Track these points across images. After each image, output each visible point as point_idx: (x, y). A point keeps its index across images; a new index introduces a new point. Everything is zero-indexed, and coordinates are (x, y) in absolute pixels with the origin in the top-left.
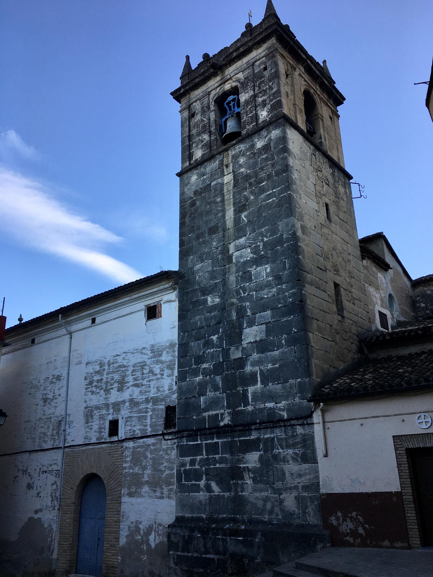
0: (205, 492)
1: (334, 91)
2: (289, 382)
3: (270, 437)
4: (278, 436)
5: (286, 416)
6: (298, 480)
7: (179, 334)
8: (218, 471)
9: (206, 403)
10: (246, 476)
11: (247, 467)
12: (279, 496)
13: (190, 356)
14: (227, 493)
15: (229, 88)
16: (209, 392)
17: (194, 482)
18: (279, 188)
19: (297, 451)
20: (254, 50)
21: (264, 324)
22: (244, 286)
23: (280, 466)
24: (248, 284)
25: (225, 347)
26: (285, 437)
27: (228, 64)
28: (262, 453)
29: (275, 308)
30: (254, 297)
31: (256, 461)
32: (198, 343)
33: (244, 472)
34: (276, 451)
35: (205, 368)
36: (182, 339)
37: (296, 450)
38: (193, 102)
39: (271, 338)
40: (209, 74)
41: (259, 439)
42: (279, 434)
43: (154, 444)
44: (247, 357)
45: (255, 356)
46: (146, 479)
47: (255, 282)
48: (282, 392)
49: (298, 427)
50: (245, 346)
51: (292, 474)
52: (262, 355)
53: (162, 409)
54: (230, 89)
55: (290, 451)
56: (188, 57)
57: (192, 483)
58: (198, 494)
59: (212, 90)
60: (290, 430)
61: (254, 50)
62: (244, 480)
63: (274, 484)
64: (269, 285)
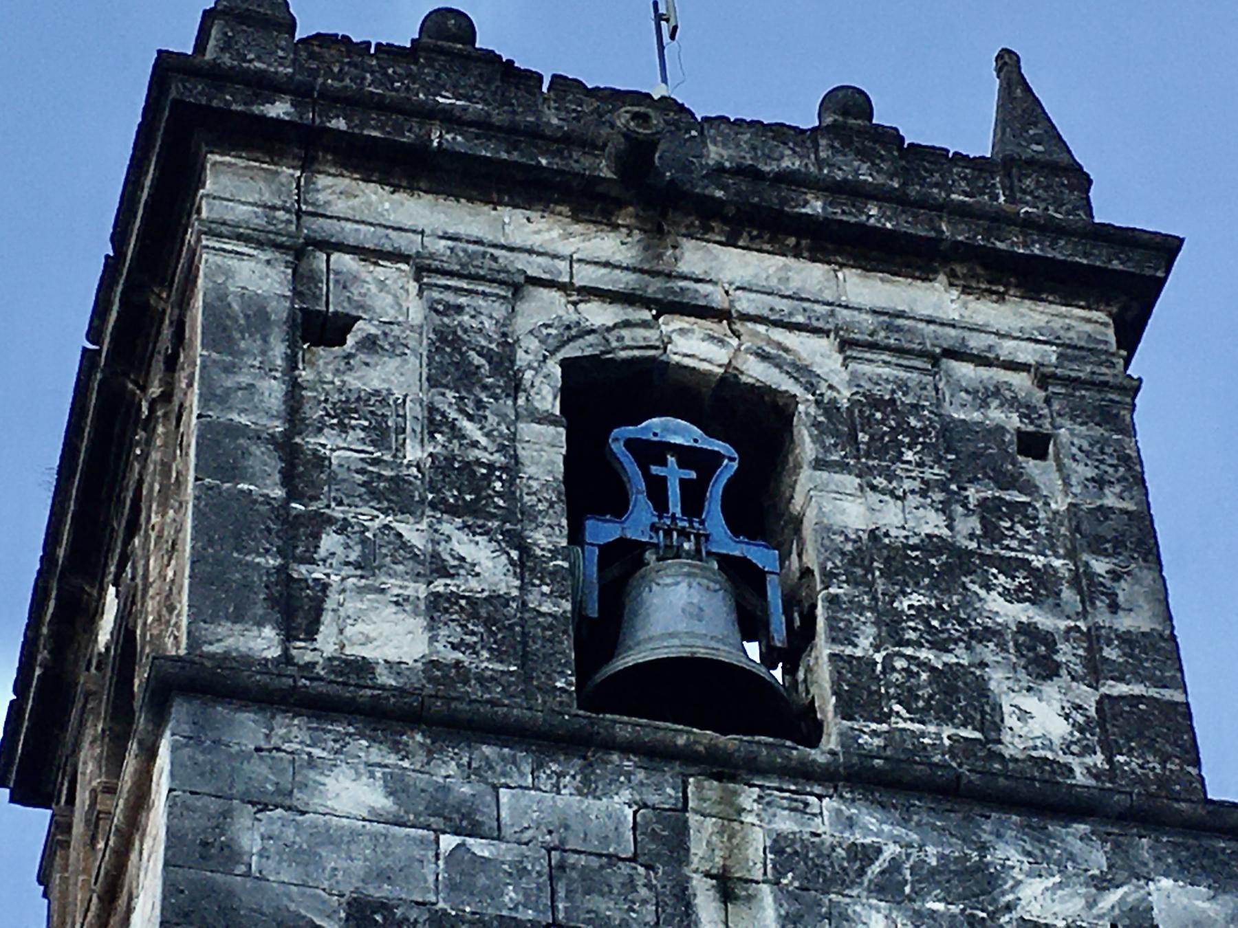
1: (61, 552)
15: (705, 366)
20: (942, 277)
27: (725, 220)
38: (351, 241)
40: (559, 172)
54: (707, 375)
56: (1008, 62)
61: (942, 277)
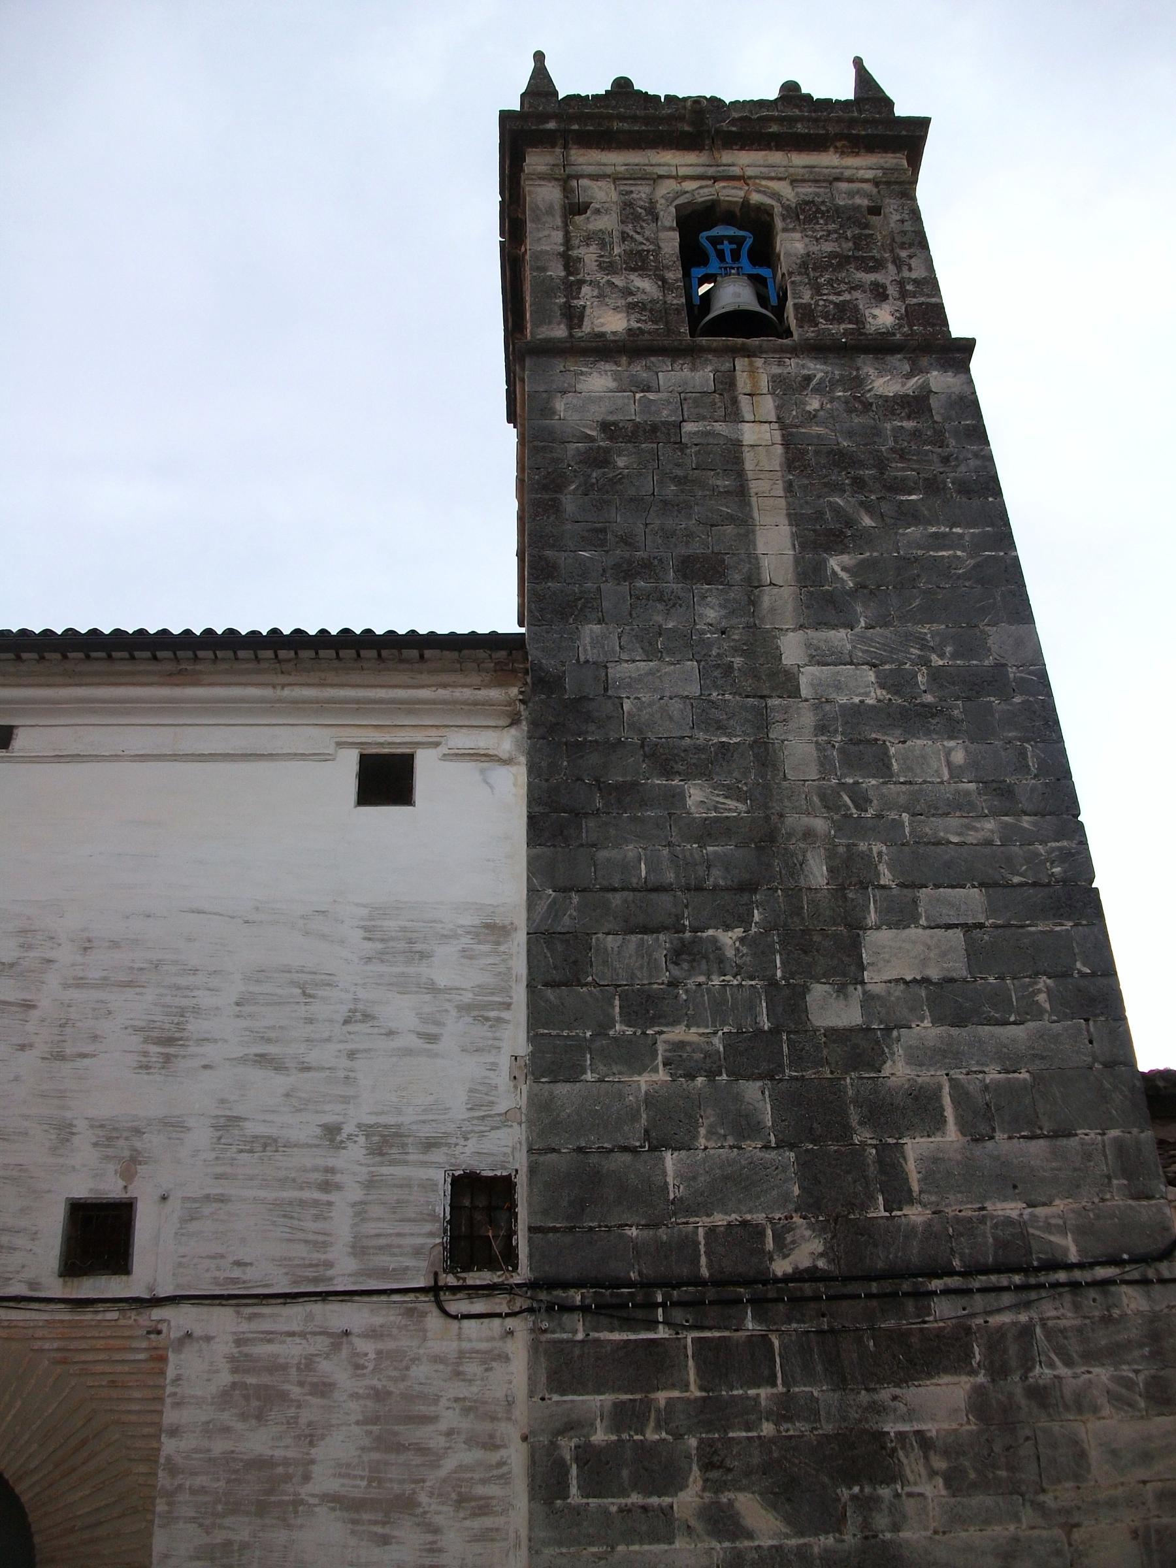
0: (706, 1538)
2: (1076, 1135)
3: (1014, 1324)
4: (1048, 1319)
5: (1073, 1249)
6: (1141, 1473)
7: (531, 890)
8: (771, 1452)
9: (694, 1178)
10: (911, 1463)
11: (918, 1433)
12: (1069, 1534)
13: (597, 985)
14: (822, 1538)
16: (708, 1140)
17: (635, 1498)
18: (977, 531)
19: (1126, 1371)
20: (832, 149)
21: (956, 926)
22: (856, 783)
23: (1061, 1427)
24: (874, 782)
25: (783, 978)
26: (1078, 1322)
28: (981, 1379)
29: (996, 885)
30: (907, 830)
31: (956, 1410)
32: (641, 943)
33: (901, 1453)
34: (1041, 1373)
35: (680, 1045)
36: (555, 910)
37: (1125, 1367)
39: (991, 980)
41: (963, 1332)
42: (1053, 1313)
43: (373, 1334)
44: (888, 1030)
45: (926, 1031)
46: (324, 1481)
47: (902, 783)
48: (1052, 1169)
49: (1124, 1288)
50: (877, 989)
51: (1114, 1453)
52: (954, 1031)
53: (429, 1186)
55: (1102, 1374)
57: (629, 1501)
58: (666, 1547)
59: (669, 177)
60: (1094, 1300)
61: (832, 149)
62: (905, 1482)
63: (1044, 1491)
64: (960, 805)
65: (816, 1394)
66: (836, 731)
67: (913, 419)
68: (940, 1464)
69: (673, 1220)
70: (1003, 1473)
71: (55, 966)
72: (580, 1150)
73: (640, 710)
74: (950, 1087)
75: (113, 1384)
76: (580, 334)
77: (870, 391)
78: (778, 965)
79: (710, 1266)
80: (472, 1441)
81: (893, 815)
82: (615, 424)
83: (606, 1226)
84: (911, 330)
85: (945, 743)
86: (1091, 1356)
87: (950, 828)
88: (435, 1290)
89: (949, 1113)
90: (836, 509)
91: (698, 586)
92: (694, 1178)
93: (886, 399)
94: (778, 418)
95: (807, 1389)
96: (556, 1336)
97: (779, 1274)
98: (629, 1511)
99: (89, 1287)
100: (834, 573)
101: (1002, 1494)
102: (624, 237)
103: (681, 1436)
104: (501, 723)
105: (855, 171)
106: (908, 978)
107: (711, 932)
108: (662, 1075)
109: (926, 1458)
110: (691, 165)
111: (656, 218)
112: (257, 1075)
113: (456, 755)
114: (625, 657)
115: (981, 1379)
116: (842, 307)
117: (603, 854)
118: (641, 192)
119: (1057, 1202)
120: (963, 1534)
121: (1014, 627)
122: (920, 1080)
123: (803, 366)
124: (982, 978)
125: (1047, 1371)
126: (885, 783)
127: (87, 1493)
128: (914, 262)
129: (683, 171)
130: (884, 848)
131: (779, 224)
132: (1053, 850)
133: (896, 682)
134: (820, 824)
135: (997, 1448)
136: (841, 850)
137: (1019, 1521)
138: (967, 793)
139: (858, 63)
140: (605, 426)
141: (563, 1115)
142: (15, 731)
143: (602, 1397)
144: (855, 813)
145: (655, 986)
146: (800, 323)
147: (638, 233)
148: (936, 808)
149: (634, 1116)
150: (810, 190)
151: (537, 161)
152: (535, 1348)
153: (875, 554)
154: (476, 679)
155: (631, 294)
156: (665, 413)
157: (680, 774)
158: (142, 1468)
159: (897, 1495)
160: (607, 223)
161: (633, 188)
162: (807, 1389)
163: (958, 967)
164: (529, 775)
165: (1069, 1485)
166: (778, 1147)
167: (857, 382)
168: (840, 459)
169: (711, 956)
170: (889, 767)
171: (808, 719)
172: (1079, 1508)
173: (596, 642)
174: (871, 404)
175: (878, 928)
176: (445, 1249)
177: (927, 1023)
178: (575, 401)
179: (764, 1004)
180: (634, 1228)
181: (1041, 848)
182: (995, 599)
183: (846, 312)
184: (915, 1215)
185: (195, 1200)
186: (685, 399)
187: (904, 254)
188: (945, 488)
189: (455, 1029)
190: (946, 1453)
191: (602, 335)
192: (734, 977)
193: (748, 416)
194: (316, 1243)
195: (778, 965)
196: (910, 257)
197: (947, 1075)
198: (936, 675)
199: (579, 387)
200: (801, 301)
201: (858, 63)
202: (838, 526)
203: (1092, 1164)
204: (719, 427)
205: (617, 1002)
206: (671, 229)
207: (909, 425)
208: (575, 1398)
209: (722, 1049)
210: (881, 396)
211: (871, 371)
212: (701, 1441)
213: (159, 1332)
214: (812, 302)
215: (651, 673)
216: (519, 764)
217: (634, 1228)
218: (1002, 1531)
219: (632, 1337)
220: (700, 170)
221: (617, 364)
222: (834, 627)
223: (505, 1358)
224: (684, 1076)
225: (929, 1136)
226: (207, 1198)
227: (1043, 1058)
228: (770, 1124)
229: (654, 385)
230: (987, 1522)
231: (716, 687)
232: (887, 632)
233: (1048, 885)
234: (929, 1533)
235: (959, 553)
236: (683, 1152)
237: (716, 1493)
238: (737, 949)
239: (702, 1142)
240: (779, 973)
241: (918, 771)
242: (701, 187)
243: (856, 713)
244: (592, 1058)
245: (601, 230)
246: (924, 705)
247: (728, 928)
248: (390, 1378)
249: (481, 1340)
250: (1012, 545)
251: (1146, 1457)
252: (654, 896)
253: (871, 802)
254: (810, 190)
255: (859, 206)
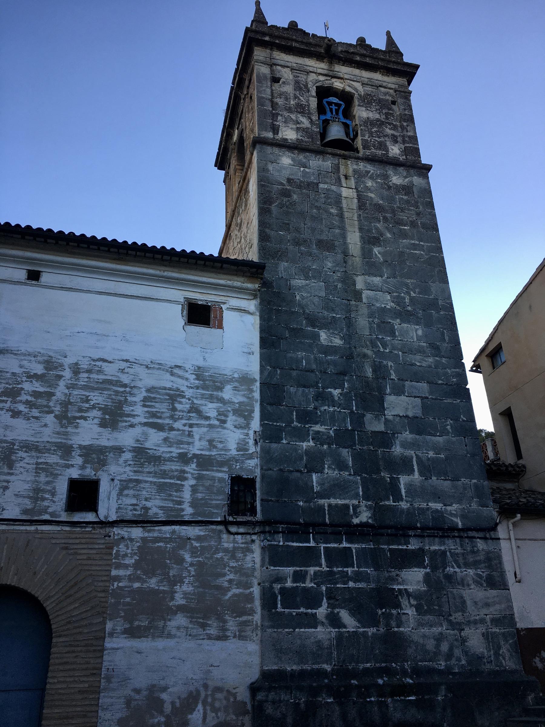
2: (461, 480)
3: (439, 550)
5: (460, 523)
7: (261, 366)
9: (323, 484)
10: (404, 602)
11: (406, 589)
14: (372, 629)
17: (302, 610)
19: (479, 572)
20: (379, 72)
21: (418, 397)
22: (383, 338)
24: (389, 338)
25: (356, 410)
26: (462, 551)
28: (428, 570)
29: (433, 383)
30: (401, 358)
31: (419, 582)
32: (303, 391)
33: (400, 597)
34: (449, 570)
35: (318, 432)
42: (453, 547)
44: (394, 434)
45: (407, 436)
46: (179, 600)
48: (452, 492)
49: (478, 540)
50: (391, 418)
51: (476, 603)
52: (417, 437)
53: (221, 480)
55: (471, 572)
57: (300, 611)
58: (314, 630)
60: (468, 543)
61: (379, 72)
62: (402, 609)
64: (420, 351)
65: (369, 572)
66: (376, 317)
67: (407, 195)
68: (413, 602)
69: (316, 500)
70: (437, 607)
71: (64, 378)
72: (281, 470)
73: (303, 299)
74: (416, 458)
75: (89, 559)
76: (277, 138)
77: (391, 181)
78: (354, 405)
79: (329, 519)
80: (239, 585)
81: (396, 352)
82: (292, 179)
83: (291, 501)
84: (406, 157)
85: (415, 326)
86: (467, 565)
87: (417, 359)
88: (225, 523)
89: (416, 467)
90: (377, 229)
91: (325, 252)
92: (323, 484)
93: (397, 185)
94: (356, 187)
95: (365, 569)
96: (272, 543)
97: (355, 523)
98: (300, 615)
99: (78, 517)
100: (376, 255)
101: (436, 615)
102: (296, 97)
103: (319, 586)
104: (250, 298)
105: (387, 84)
106: (401, 415)
107: (329, 390)
108: (311, 443)
109: (409, 599)
110: (322, 69)
111: (308, 91)
112: (152, 431)
113: (232, 309)
114: (296, 277)
115: (428, 570)
116: (380, 143)
117: (289, 355)
118: (302, 78)
119: (454, 505)
120: (423, 630)
121: (441, 285)
122: (405, 454)
123: (365, 167)
124: (427, 418)
125: (451, 569)
126: (393, 339)
127: (77, 606)
128: (409, 128)
129: (319, 71)
130: (392, 364)
131: (356, 102)
132: (453, 372)
133: (398, 301)
134: (369, 352)
135: (434, 597)
136: (377, 363)
137: (443, 627)
138: (423, 347)
139: (388, 34)
140: (289, 180)
141: (274, 456)
142: (41, 274)
143: (290, 568)
144: (382, 350)
145: (309, 409)
146: (364, 148)
147: (301, 96)
148: (412, 351)
149: (301, 459)
150: (370, 89)
151: (259, 53)
152: (263, 548)
153: (391, 249)
154: (242, 279)
155: (298, 123)
156: (312, 178)
157: (318, 327)
158: (102, 595)
159: (399, 614)
160: (289, 89)
161: (299, 75)
162: (365, 569)
163: (419, 412)
164: (260, 320)
165: (460, 614)
166: (354, 475)
167: (386, 177)
168: (379, 208)
169: (329, 399)
170: (395, 333)
171: (364, 310)
172: (464, 623)
173: (285, 270)
174: (391, 187)
175: (390, 395)
176: (228, 506)
177: (407, 433)
178: (277, 167)
179: (349, 420)
180: (301, 502)
181: (449, 371)
182: (435, 272)
183: (382, 146)
184: (404, 505)
185: (125, 481)
186: (320, 174)
187: (405, 124)
188: (418, 226)
189: (231, 419)
190: (415, 598)
191: (286, 139)
192: (338, 408)
193: (345, 185)
194: (176, 501)
195: (354, 405)
196: (408, 126)
197: (415, 453)
198: (412, 299)
199: (278, 161)
200: (364, 138)
201: (388, 34)
202: (378, 236)
203: (466, 492)
204: (334, 188)
205: (295, 413)
206: (313, 97)
207: (405, 197)
208: (280, 568)
209: (333, 435)
210: (395, 184)
211: (392, 173)
212: (327, 588)
213: (110, 536)
214: (369, 139)
215: (307, 285)
216: (256, 315)
217: (301, 502)
218: (436, 630)
219: (301, 545)
220: (325, 72)
221: (293, 153)
222: (376, 276)
223: (252, 552)
224: (320, 444)
225: (408, 476)
226: (131, 480)
227: (449, 450)
228: (351, 466)
229: (308, 165)
230: (431, 626)
231: (332, 294)
232: (395, 280)
233: (451, 385)
234: (410, 629)
235: (422, 253)
236: (319, 474)
237: (333, 609)
238: (339, 397)
239: (326, 471)
240: (354, 408)
241: (405, 336)
242: (327, 80)
243: (383, 310)
244: (285, 435)
245: (285, 91)
246: (408, 311)
247: (335, 389)
248: (206, 558)
249: (242, 543)
250: (442, 252)
251: (487, 605)
252: (308, 373)
253: (388, 346)
254: (370, 89)
255: (388, 100)
